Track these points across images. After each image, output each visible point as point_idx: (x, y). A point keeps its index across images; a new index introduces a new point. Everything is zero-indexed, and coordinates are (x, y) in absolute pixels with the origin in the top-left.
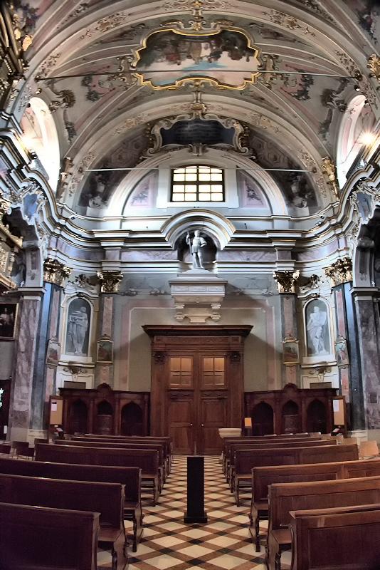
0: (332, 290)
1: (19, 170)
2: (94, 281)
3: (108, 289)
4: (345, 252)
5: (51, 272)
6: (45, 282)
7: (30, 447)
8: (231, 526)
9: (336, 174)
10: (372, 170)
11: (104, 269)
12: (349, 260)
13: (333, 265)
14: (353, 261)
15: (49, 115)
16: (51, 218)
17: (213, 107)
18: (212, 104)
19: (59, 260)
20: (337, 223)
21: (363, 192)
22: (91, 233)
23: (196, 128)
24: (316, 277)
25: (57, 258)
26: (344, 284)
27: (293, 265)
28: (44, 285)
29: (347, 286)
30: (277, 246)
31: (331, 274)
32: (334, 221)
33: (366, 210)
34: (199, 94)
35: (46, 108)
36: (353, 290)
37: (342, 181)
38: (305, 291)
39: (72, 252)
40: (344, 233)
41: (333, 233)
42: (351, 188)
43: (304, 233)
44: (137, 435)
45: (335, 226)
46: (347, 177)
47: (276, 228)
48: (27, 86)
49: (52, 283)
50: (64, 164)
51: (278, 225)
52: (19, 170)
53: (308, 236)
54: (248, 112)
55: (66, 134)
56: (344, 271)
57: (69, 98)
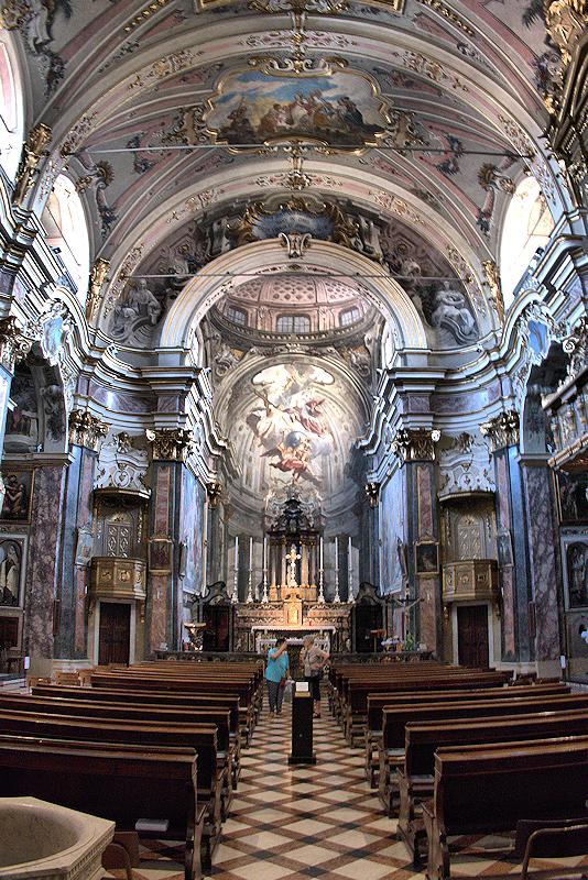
0: (490, 456)
1: (41, 290)
2: (138, 443)
3: (162, 455)
4: (511, 402)
5: (80, 430)
6: (71, 445)
7: (539, 364)
8: (334, 839)
9: (500, 287)
10: (546, 292)
11: (156, 424)
12: (515, 414)
13: (494, 421)
14: (521, 417)
15: (75, 197)
16: (211, 437)
17: (319, 181)
18: (318, 175)
19: (92, 413)
20: (500, 359)
21: (537, 321)
22: (140, 373)
23: (302, 223)
24: (466, 436)
25: (89, 410)
26: (508, 447)
27: (431, 419)
28: (70, 450)
29: (513, 453)
30: (410, 391)
31: (490, 434)
32: (495, 356)
33: (541, 346)
34: (303, 17)
35: (71, 187)
36: (520, 458)
37: (509, 299)
38: (449, 458)
39: (111, 399)
40: (508, 373)
41: (494, 373)
42: (519, 312)
43: (449, 372)
44: (156, 713)
45: (495, 364)
46: (515, 294)
47: (410, 366)
48: (50, 163)
49: (82, 447)
50: (95, 263)
51: (413, 362)
52: (41, 290)
53: (455, 377)
54: (400, 51)
55: (100, 222)
56: (509, 430)
57: (105, 173)
